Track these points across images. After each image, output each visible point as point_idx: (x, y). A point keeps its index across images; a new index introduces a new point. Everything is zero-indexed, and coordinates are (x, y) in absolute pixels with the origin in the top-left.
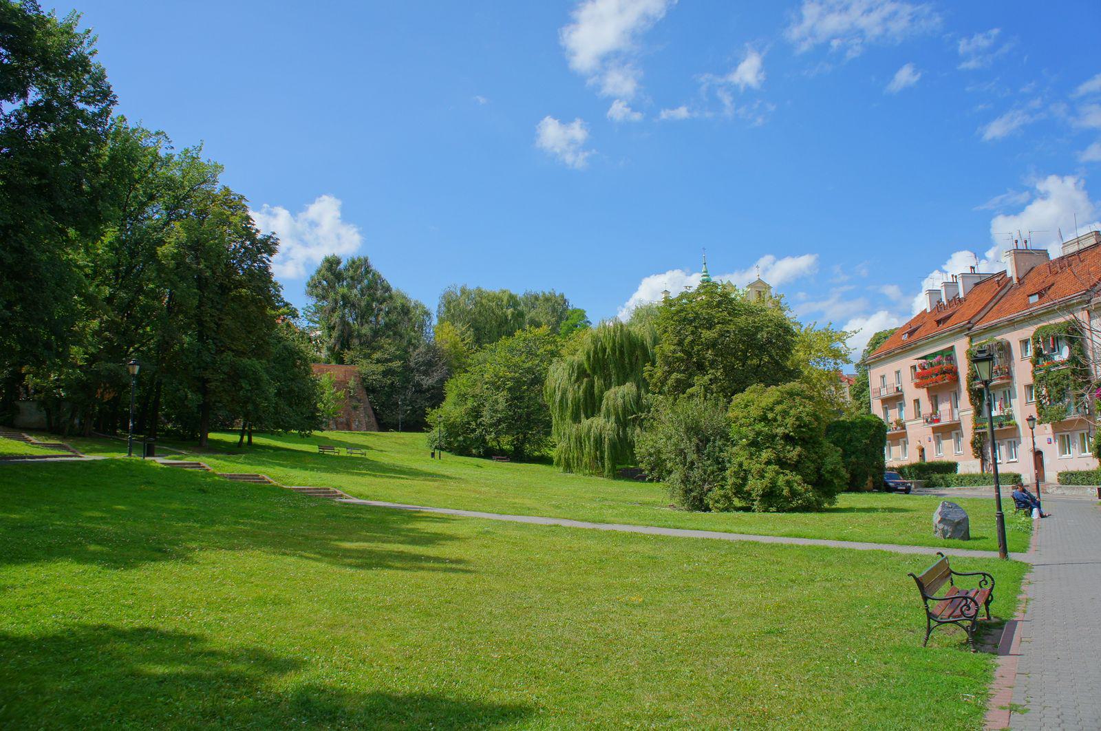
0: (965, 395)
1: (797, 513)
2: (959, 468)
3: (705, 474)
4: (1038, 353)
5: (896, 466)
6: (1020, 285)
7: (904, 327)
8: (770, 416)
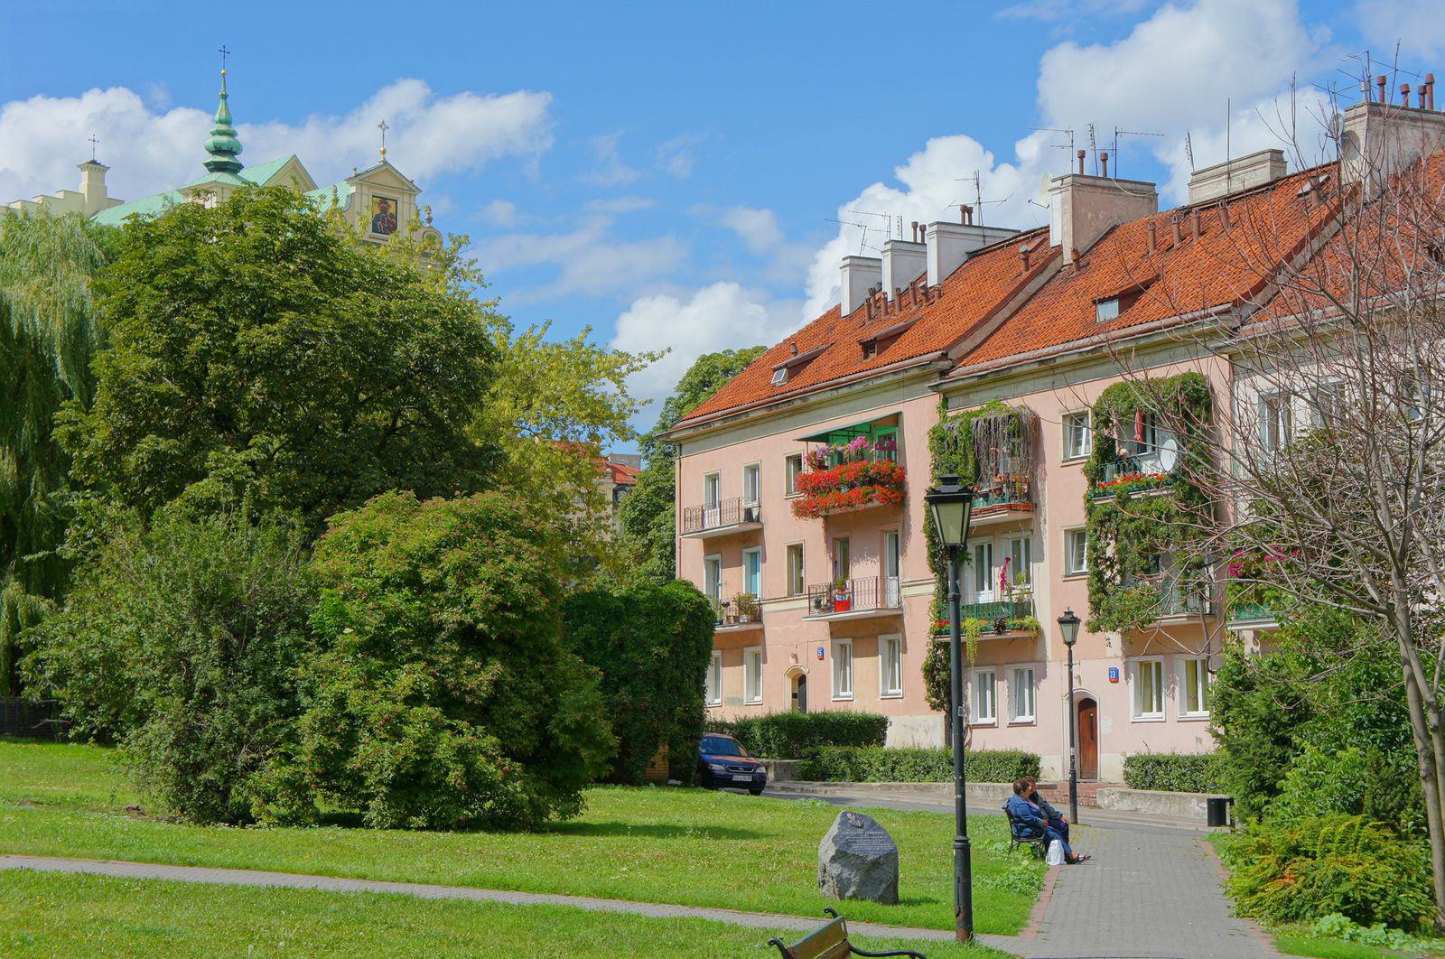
0: (917, 545)
1: (481, 835)
2: (891, 733)
3: (243, 723)
4: (1105, 452)
5: (730, 719)
6: (1079, 268)
7: (779, 349)
8: (428, 575)
